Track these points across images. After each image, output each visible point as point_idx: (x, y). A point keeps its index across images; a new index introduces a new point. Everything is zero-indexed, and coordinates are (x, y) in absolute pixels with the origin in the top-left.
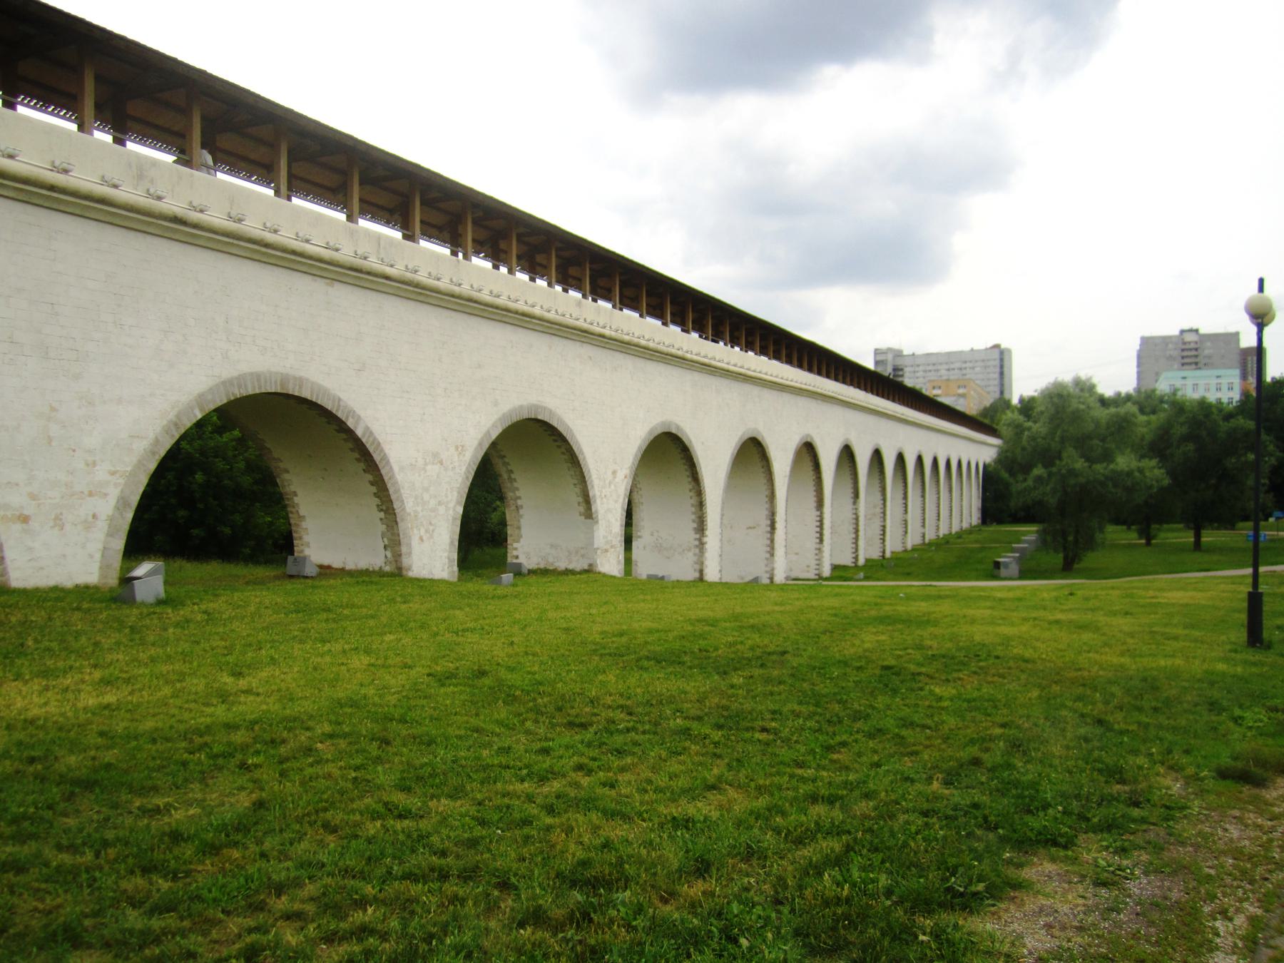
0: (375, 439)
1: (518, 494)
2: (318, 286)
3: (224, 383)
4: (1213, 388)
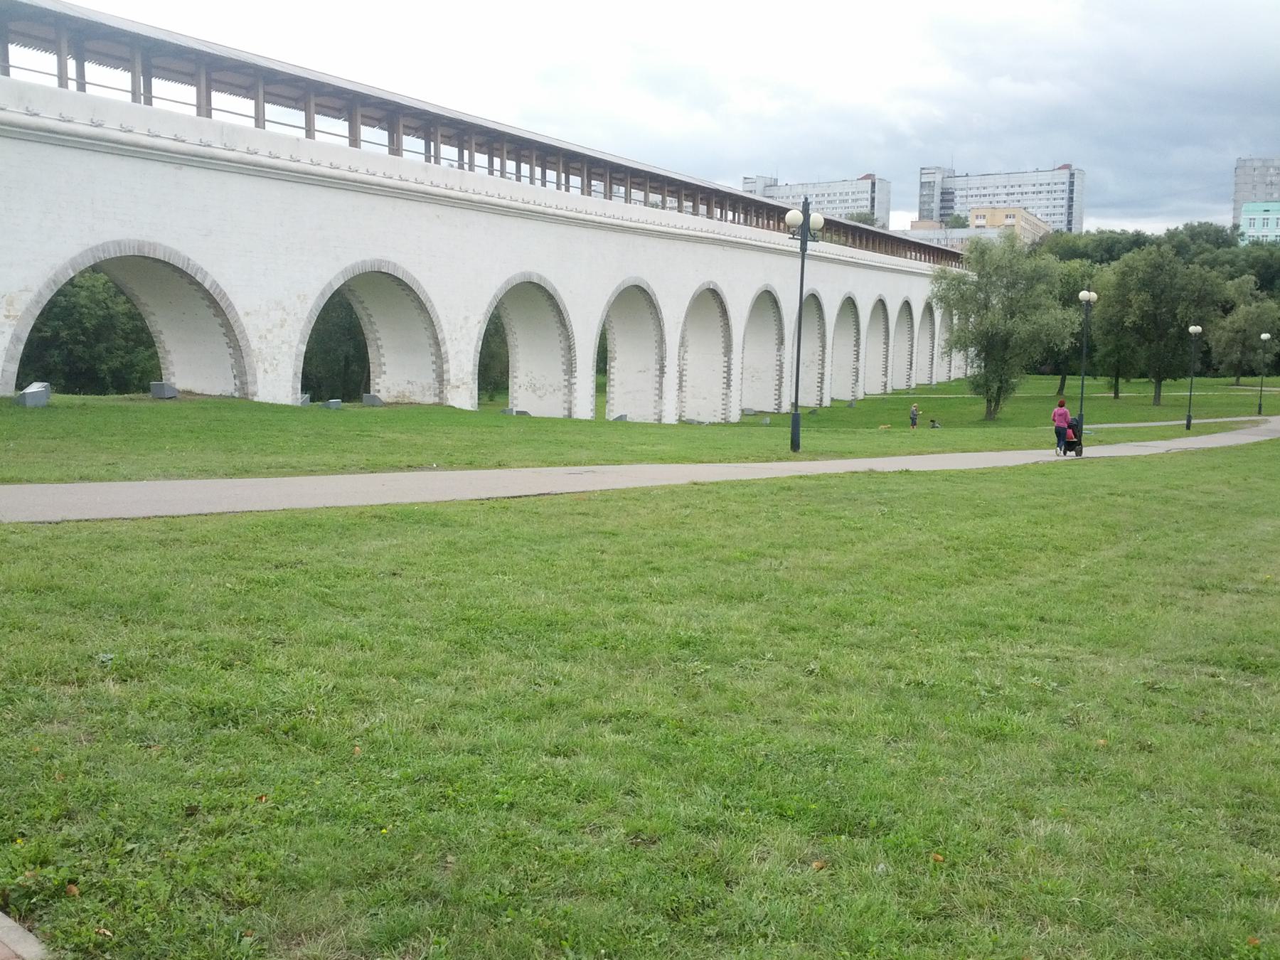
0: (221, 290)
1: (378, 335)
2: (168, 170)
3: (91, 249)
4: (1258, 223)
